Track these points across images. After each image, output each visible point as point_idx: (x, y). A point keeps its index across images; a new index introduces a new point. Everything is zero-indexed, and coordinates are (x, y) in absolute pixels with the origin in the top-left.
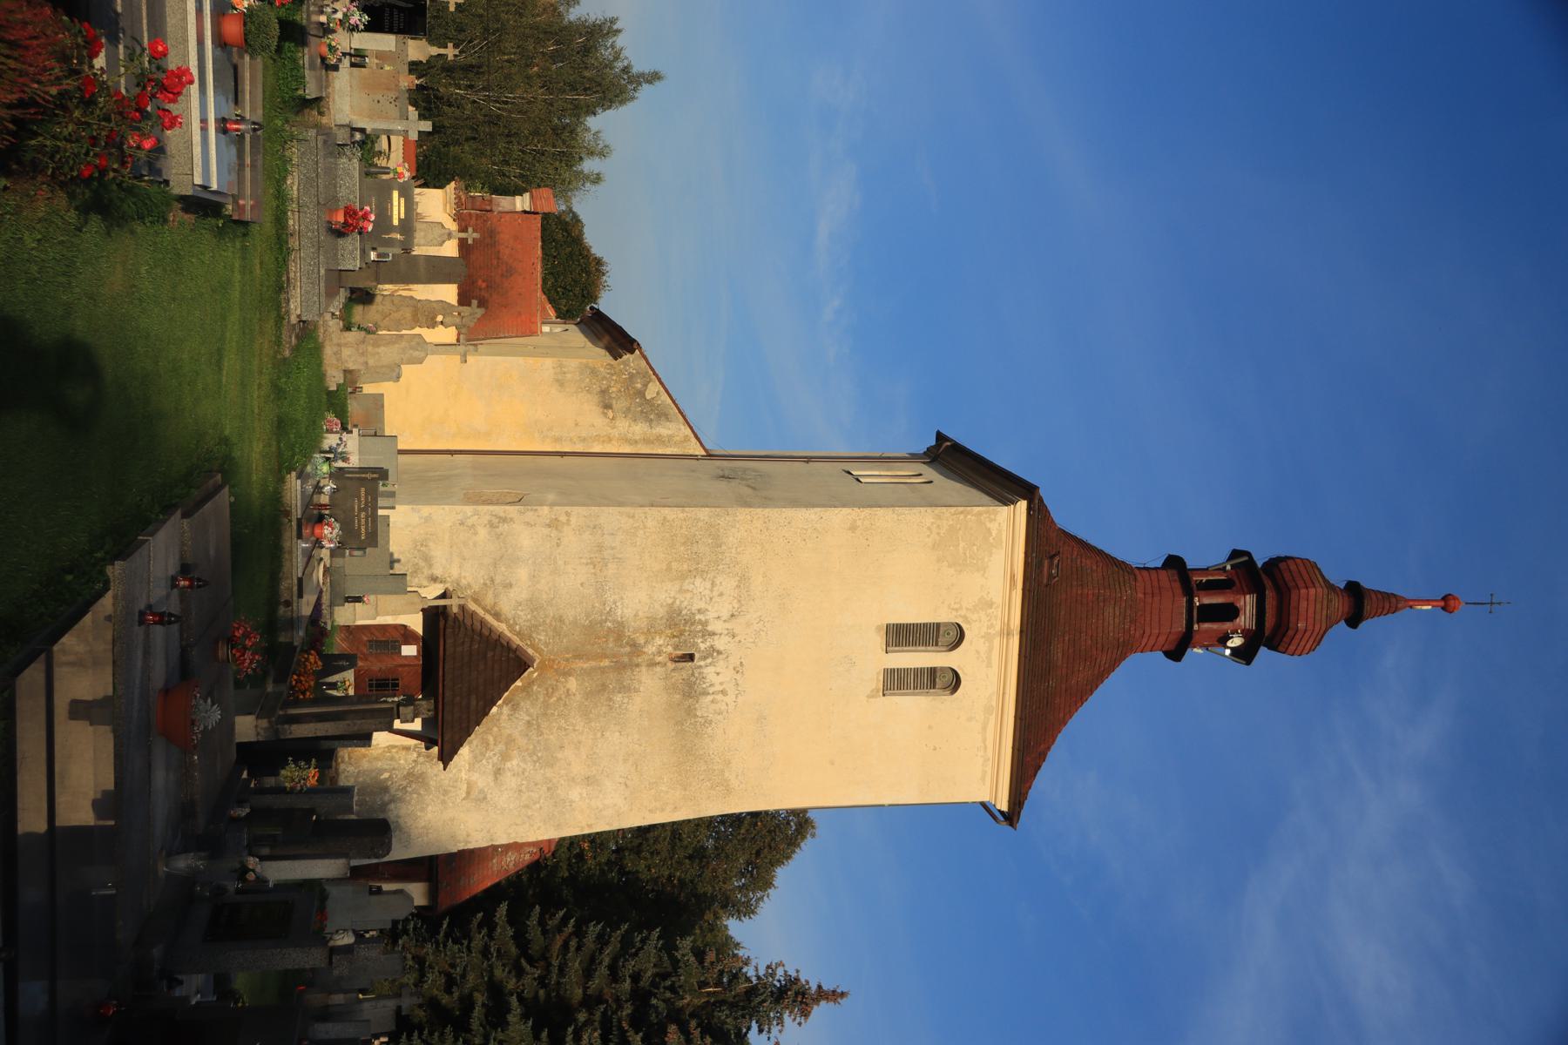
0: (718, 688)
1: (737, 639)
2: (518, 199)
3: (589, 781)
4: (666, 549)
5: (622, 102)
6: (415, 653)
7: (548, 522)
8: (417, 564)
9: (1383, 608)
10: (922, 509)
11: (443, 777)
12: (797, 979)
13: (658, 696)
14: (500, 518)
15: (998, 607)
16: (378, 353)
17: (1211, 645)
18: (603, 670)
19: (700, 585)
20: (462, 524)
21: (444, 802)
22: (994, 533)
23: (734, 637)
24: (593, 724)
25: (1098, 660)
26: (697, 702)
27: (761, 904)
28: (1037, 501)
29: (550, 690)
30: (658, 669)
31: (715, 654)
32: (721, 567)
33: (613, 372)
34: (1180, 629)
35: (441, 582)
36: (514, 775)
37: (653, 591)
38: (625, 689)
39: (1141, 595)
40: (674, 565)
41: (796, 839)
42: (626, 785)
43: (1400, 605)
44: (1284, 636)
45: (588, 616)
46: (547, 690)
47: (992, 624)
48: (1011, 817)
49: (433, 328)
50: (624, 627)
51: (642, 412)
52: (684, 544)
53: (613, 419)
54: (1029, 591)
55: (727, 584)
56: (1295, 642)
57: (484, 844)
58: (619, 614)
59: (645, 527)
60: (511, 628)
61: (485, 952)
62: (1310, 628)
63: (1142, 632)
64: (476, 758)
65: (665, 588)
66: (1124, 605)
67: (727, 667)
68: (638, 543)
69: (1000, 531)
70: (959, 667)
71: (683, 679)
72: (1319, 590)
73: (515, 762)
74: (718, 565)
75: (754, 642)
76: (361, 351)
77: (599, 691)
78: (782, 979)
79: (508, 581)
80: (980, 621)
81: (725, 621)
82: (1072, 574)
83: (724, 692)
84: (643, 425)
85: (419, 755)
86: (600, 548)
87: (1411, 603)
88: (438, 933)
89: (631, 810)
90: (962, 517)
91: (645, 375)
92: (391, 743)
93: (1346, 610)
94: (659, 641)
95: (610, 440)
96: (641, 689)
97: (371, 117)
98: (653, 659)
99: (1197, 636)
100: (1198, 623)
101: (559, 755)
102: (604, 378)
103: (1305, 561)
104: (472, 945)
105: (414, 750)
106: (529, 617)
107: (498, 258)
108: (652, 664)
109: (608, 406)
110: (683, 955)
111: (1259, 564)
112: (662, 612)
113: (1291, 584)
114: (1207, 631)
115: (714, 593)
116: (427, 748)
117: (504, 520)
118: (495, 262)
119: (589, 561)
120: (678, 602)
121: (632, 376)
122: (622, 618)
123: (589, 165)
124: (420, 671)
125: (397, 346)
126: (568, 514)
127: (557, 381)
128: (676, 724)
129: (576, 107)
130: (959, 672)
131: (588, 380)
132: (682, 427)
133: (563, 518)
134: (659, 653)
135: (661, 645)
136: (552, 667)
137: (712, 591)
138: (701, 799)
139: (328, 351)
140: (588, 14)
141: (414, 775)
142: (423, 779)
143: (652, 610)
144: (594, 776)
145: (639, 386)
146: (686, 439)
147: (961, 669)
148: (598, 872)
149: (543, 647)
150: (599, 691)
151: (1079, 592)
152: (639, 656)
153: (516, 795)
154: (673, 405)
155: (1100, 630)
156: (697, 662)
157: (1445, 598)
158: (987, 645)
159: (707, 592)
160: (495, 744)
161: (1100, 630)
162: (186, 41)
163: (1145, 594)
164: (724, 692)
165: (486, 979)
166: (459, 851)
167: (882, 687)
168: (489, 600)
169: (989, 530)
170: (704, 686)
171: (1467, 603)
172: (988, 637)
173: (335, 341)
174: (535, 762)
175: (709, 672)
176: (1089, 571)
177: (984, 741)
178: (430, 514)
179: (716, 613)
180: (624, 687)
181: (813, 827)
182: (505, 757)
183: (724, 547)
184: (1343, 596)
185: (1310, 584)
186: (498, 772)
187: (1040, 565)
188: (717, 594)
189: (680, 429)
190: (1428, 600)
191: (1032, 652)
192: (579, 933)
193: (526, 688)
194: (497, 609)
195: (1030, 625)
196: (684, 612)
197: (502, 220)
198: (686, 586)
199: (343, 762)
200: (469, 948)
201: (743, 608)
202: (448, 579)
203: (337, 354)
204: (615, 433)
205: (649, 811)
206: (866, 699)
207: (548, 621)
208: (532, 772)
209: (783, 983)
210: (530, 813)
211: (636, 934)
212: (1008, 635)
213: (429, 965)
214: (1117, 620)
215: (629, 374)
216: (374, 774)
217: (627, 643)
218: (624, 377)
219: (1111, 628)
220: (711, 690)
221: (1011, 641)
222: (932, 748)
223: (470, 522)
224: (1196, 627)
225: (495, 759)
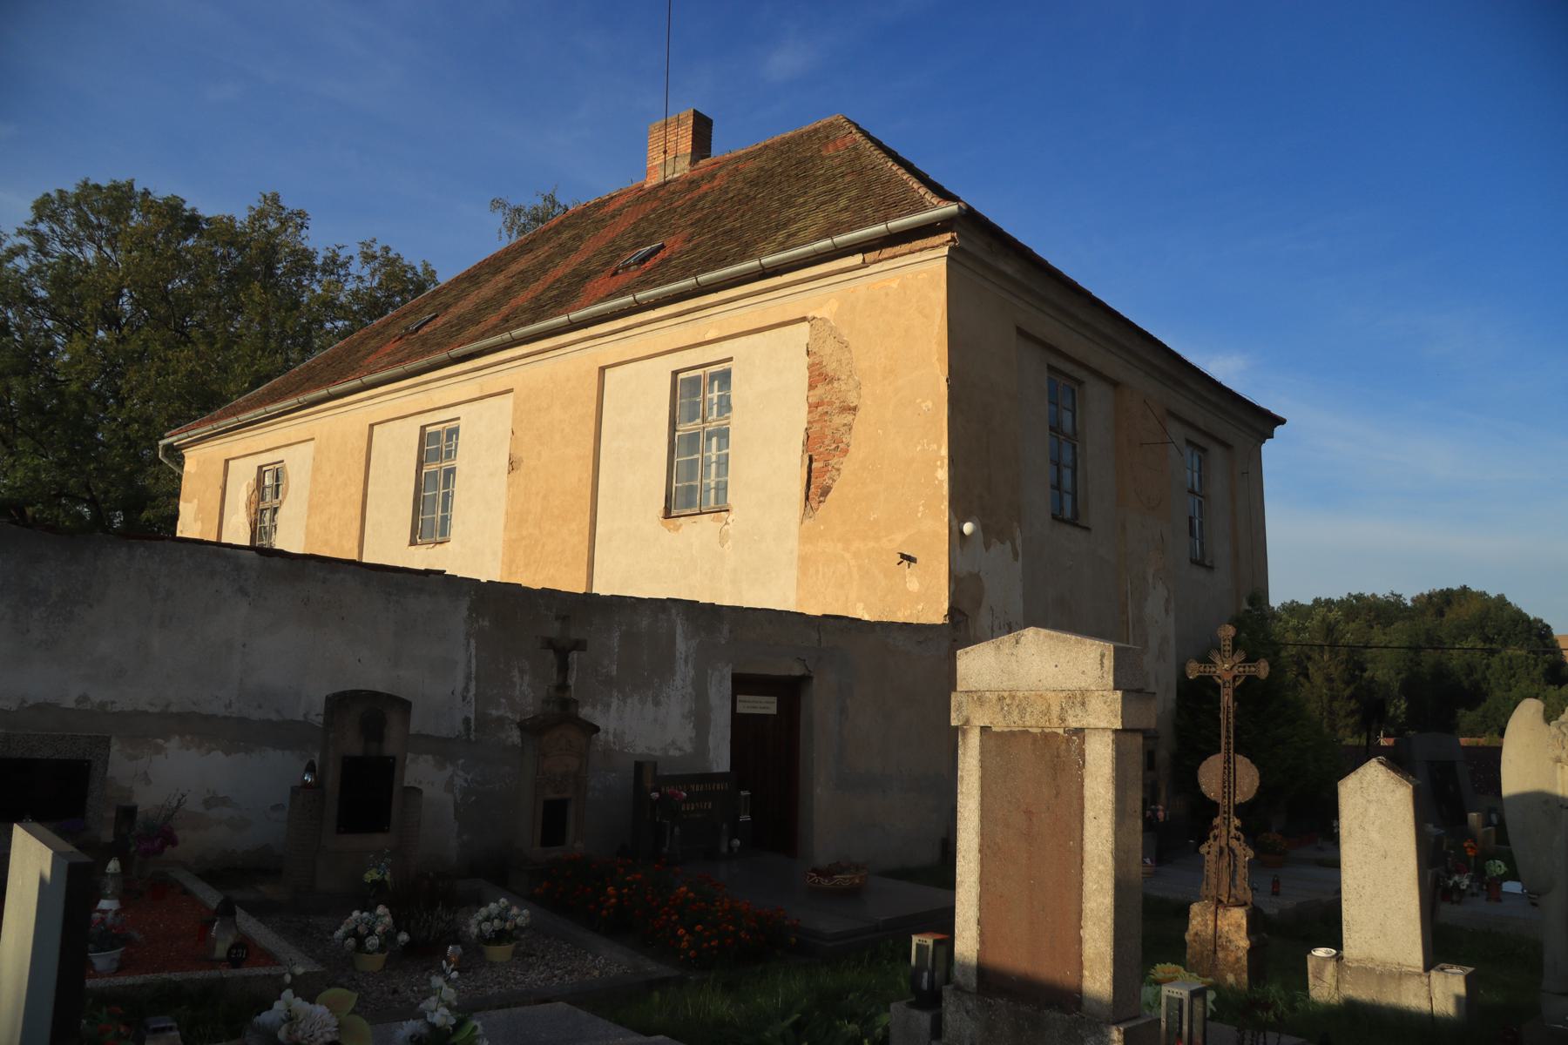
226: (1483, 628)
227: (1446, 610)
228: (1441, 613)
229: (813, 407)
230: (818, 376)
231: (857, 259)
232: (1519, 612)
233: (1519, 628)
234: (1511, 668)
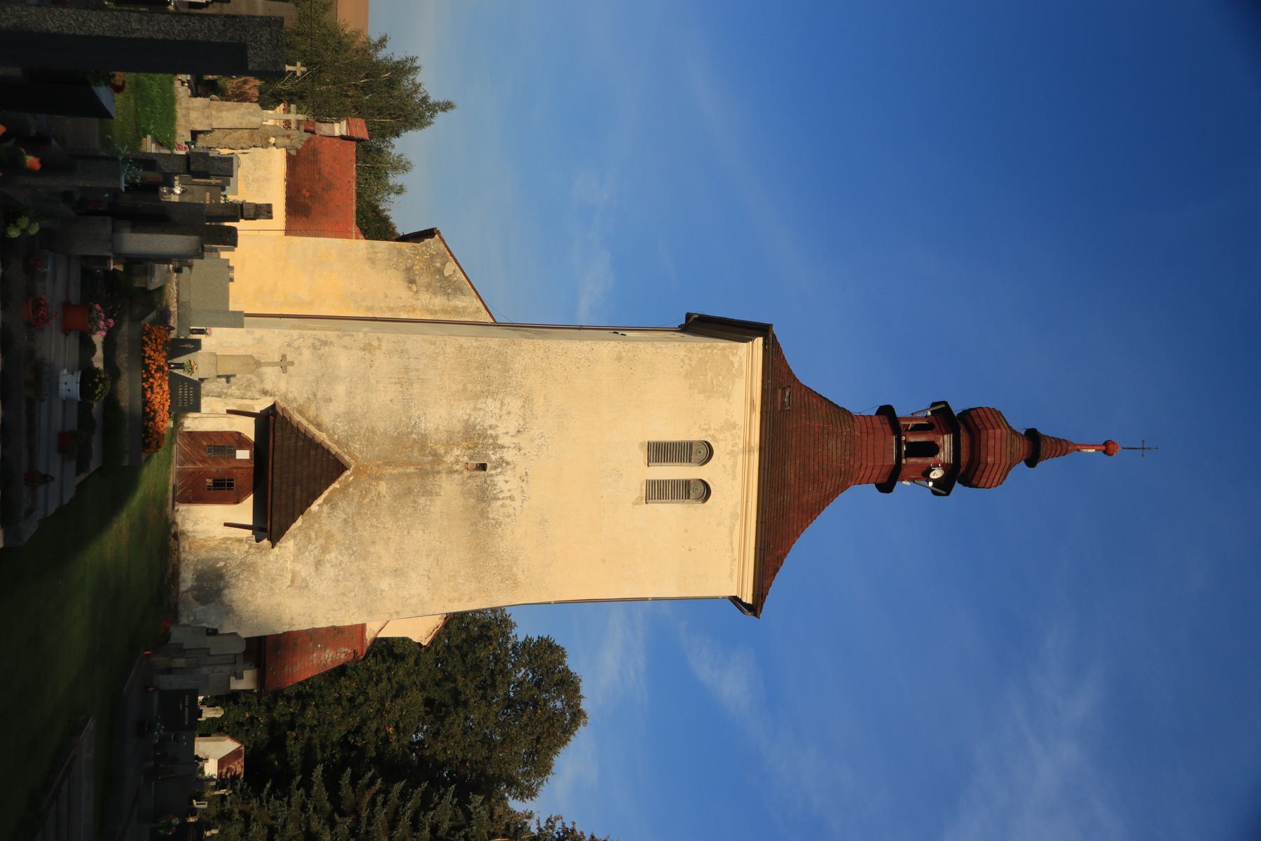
1: (522, 452)
2: (337, 126)
3: (397, 573)
4: (463, 372)
5: (422, 126)
6: (248, 457)
7: (362, 346)
8: (250, 379)
9: (1056, 450)
10: (677, 344)
11: (271, 567)
12: (573, 830)
13: (456, 499)
14: (322, 341)
15: (740, 428)
16: (221, 117)
17: (916, 479)
18: (409, 476)
19: (491, 405)
20: (289, 345)
21: (271, 589)
22: (736, 365)
23: (520, 450)
24: (400, 523)
25: (825, 484)
26: (489, 506)
27: (541, 788)
28: (771, 336)
29: (364, 492)
30: (456, 476)
31: (504, 464)
32: (509, 389)
33: (416, 253)
34: (891, 463)
35: (271, 395)
36: (332, 566)
37: (451, 408)
38: (428, 493)
39: (857, 433)
40: (469, 386)
41: (571, 727)
42: (429, 578)
43: (1070, 448)
44: (976, 470)
45: (396, 428)
46: (361, 492)
47: (736, 443)
48: (754, 609)
49: (267, 148)
50: (427, 439)
51: (441, 287)
52: (477, 368)
53: (417, 292)
54: (767, 413)
55: (514, 404)
56: (986, 474)
58: (422, 427)
59: (445, 353)
60: (330, 437)
61: (304, 808)
62: (997, 462)
63: (859, 464)
64: (300, 551)
65: (462, 406)
66: (844, 439)
67: (514, 476)
68: (439, 367)
69: (741, 364)
70: (709, 479)
71: (477, 486)
72: (1004, 430)
73: (333, 555)
74: (506, 388)
75: (537, 455)
76: (206, 115)
77: (405, 494)
78: (560, 830)
79: (328, 396)
80: (726, 440)
81: (512, 436)
82: (801, 407)
83: (511, 498)
84: (442, 298)
85: (251, 546)
86: (407, 370)
87: (1079, 447)
88: (262, 792)
89: (433, 599)
90: (709, 351)
91: (443, 256)
92: (226, 536)
93: (1026, 451)
94: (457, 452)
95: (414, 310)
96: (442, 493)
98: (451, 467)
99: (905, 470)
100: (905, 458)
101: (372, 550)
102: (409, 258)
103: (992, 410)
104: (291, 800)
105: (246, 542)
106: (346, 427)
107: (320, 174)
108: (451, 472)
110: (475, 808)
111: (956, 414)
112: (459, 427)
113: (981, 427)
114: (913, 465)
115: (503, 412)
116: (258, 541)
117: (325, 343)
118: (317, 177)
119: (397, 381)
120: (472, 419)
121: (432, 256)
122: (425, 431)
123: (394, 179)
124: (252, 473)
125: (237, 111)
126: (379, 339)
127: (370, 259)
128: (472, 524)
129: (383, 128)
130: (709, 483)
131: (395, 259)
132: (475, 300)
133: (375, 343)
134: (457, 462)
136: (365, 472)
137: (501, 410)
138: (493, 591)
139: (180, 112)
140: (393, 54)
141: (245, 564)
142: (254, 568)
143: (451, 425)
144: (401, 569)
145: (438, 265)
146: (478, 311)
147: (709, 481)
148: (401, 754)
149: (358, 454)
150: (405, 494)
151: (808, 423)
152: (439, 464)
153: (334, 584)
154: (467, 282)
155: (825, 459)
156: (489, 471)
157: (1106, 444)
158: (732, 460)
159: (497, 411)
160: (316, 539)
161: (825, 459)
163: (861, 432)
164: (511, 498)
165: (304, 829)
166: (284, 633)
167: (645, 496)
168: (312, 412)
169: (732, 363)
170: (495, 492)
171: (1123, 448)
172: (732, 454)
173: (184, 105)
174: (351, 555)
175: (499, 480)
176: (815, 407)
177: (731, 543)
178: (262, 336)
179: (505, 430)
180: (427, 491)
181: (585, 716)
182: (325, 550)
183: (511, 372)
184: (1023, 439)
185: (996, 426)
186: (318, 564)
187: (774, 391)
188: (506, 412)
189: (473, 302)
190: (1093, 445)
191: (770, 465)
192: (386, 791)
193: (344, 489)
194: (319, 420)
195: (767, 441)
196: (478, 427)
197: (323, 142)
198: (479, 405)
199: (184, 551)
200: (289, 804)
201: (528, 426)
202: (277, 393)
203: (186, 116)
204: (418, 304)
205: (449, 600)
206: (632, 506)
207: (362, 433)
208: (348, 563)
209: (561, 834)
210: (346, 600)
211: (434, 794)
212: (749, 451)
213: (254, 819)
214: (839, 452)
215: (430, 254)
217: (430, 453)
218: (426, 257)
219: (834, 458)
220: (501, 496)
221: (752, 457)
222: (688, 548)
223: (296, 344)
224: (904, 461)
225: (316, 552)
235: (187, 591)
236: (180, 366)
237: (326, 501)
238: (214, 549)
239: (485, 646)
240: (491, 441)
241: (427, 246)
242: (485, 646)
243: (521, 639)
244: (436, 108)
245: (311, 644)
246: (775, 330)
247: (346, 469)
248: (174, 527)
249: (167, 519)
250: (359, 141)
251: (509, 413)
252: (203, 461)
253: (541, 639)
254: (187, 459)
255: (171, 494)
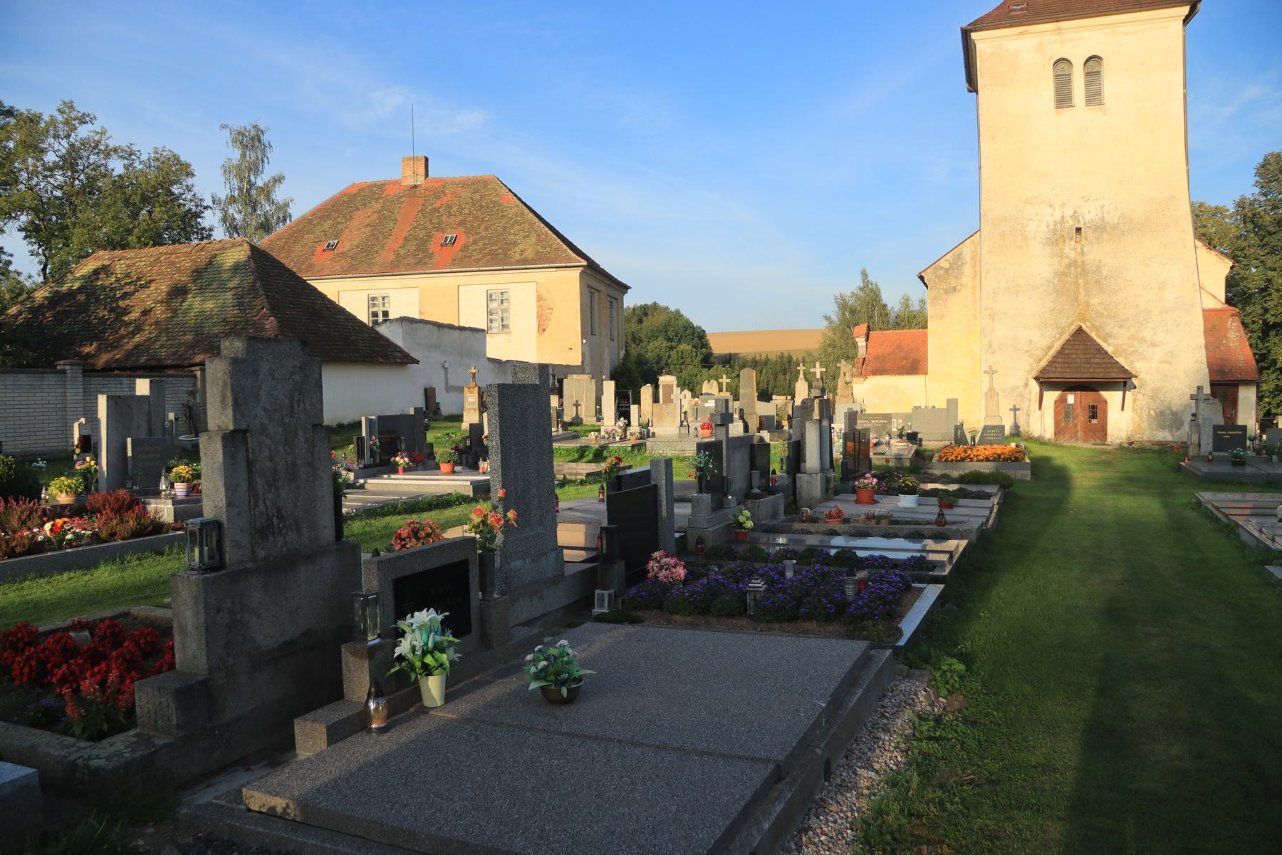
0: (1099, 211)
5: (878, 289)
18: (1086, 283)
30: (1085, 249)
38: (1099, 268)
53: (962, 285)
57: (1204, 352)
60: (1056, 340)
73: (1147, 335)
83: (1102, 207)
85: (1140, 392)
90: (983, 72)
91: (936, 268)
94: (1067, 250)
97: (675, 417)
108: (1082, 253)
109: (955, 289)
116: (1135, 388)
120: (1042, 240)
121: (936, 276)
126: (986, 309)
133: (989, 312)
135: (1070, 250)
162: (419, 485)
164: (1102, 207)
166: (1208, 367)
168: (1040, 353)
175: (1088, 217)
182: (1143, 340)
186: (1153, 345)
187: (1011, 18)
196: (1048, 236)
207: (1053, 318)
212: (1060, 30)
216: (1151, 420)
226: (666, 332)
227: (644, 318)
228: (640, 321)
229: (538, 307)
230: (540, 299)
231: (554, 269)
232: (688, 322)
233: (687, 332)
234: (682, 358)
235: (1173, 437)
236: (973, 439)
237: (1105, 341)
238: (1141, 418)
239: (1261, 217)
240: (1059, 226)
241: (930, 280)
242: (1261, 217)
243: (1257, 190)
244: (866, 282)
245: (1222, 348)
246: (965, 24)
247: (1081, 327)
248: (1123, 445)
249: (1117, 449)
250: (869, 329)
251: (1037, 214)
252: (1076, 426)
253: (1258, 174)
254: (1075, 436)
255: (1098, 447)
